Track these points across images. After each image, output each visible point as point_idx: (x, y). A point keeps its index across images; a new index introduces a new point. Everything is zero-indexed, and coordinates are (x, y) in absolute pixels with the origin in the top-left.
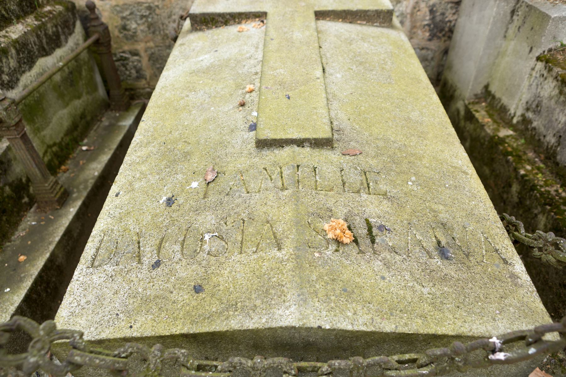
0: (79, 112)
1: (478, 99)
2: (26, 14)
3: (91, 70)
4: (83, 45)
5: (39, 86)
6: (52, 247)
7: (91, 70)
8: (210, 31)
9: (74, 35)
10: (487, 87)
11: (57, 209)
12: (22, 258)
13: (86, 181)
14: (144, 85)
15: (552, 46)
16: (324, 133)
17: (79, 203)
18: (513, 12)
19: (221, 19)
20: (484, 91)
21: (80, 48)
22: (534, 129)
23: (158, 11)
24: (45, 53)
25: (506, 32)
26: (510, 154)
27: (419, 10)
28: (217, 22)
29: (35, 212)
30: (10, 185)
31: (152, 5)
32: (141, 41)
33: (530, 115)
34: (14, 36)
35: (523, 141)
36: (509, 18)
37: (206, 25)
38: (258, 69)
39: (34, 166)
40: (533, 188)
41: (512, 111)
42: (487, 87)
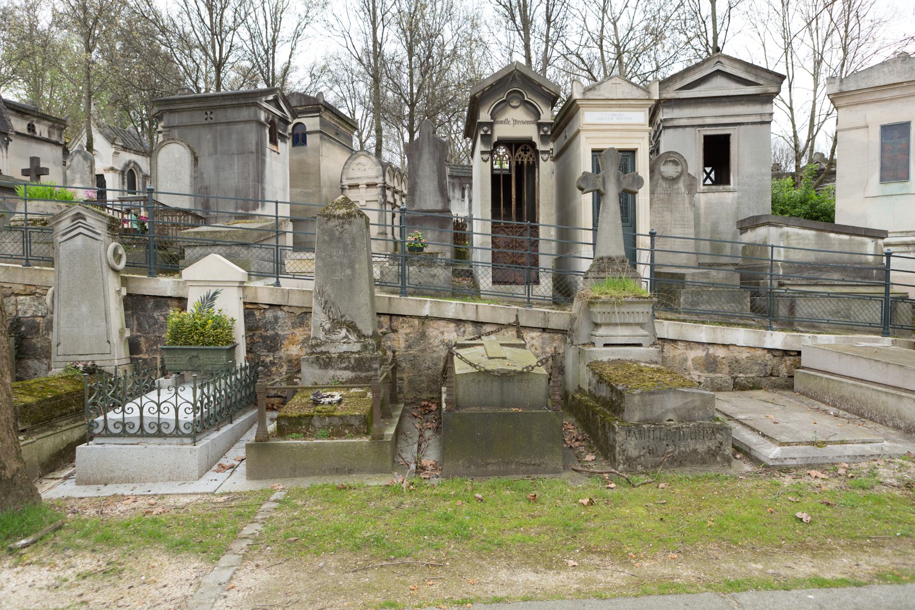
1: (577, 392)
42: (579, 386)
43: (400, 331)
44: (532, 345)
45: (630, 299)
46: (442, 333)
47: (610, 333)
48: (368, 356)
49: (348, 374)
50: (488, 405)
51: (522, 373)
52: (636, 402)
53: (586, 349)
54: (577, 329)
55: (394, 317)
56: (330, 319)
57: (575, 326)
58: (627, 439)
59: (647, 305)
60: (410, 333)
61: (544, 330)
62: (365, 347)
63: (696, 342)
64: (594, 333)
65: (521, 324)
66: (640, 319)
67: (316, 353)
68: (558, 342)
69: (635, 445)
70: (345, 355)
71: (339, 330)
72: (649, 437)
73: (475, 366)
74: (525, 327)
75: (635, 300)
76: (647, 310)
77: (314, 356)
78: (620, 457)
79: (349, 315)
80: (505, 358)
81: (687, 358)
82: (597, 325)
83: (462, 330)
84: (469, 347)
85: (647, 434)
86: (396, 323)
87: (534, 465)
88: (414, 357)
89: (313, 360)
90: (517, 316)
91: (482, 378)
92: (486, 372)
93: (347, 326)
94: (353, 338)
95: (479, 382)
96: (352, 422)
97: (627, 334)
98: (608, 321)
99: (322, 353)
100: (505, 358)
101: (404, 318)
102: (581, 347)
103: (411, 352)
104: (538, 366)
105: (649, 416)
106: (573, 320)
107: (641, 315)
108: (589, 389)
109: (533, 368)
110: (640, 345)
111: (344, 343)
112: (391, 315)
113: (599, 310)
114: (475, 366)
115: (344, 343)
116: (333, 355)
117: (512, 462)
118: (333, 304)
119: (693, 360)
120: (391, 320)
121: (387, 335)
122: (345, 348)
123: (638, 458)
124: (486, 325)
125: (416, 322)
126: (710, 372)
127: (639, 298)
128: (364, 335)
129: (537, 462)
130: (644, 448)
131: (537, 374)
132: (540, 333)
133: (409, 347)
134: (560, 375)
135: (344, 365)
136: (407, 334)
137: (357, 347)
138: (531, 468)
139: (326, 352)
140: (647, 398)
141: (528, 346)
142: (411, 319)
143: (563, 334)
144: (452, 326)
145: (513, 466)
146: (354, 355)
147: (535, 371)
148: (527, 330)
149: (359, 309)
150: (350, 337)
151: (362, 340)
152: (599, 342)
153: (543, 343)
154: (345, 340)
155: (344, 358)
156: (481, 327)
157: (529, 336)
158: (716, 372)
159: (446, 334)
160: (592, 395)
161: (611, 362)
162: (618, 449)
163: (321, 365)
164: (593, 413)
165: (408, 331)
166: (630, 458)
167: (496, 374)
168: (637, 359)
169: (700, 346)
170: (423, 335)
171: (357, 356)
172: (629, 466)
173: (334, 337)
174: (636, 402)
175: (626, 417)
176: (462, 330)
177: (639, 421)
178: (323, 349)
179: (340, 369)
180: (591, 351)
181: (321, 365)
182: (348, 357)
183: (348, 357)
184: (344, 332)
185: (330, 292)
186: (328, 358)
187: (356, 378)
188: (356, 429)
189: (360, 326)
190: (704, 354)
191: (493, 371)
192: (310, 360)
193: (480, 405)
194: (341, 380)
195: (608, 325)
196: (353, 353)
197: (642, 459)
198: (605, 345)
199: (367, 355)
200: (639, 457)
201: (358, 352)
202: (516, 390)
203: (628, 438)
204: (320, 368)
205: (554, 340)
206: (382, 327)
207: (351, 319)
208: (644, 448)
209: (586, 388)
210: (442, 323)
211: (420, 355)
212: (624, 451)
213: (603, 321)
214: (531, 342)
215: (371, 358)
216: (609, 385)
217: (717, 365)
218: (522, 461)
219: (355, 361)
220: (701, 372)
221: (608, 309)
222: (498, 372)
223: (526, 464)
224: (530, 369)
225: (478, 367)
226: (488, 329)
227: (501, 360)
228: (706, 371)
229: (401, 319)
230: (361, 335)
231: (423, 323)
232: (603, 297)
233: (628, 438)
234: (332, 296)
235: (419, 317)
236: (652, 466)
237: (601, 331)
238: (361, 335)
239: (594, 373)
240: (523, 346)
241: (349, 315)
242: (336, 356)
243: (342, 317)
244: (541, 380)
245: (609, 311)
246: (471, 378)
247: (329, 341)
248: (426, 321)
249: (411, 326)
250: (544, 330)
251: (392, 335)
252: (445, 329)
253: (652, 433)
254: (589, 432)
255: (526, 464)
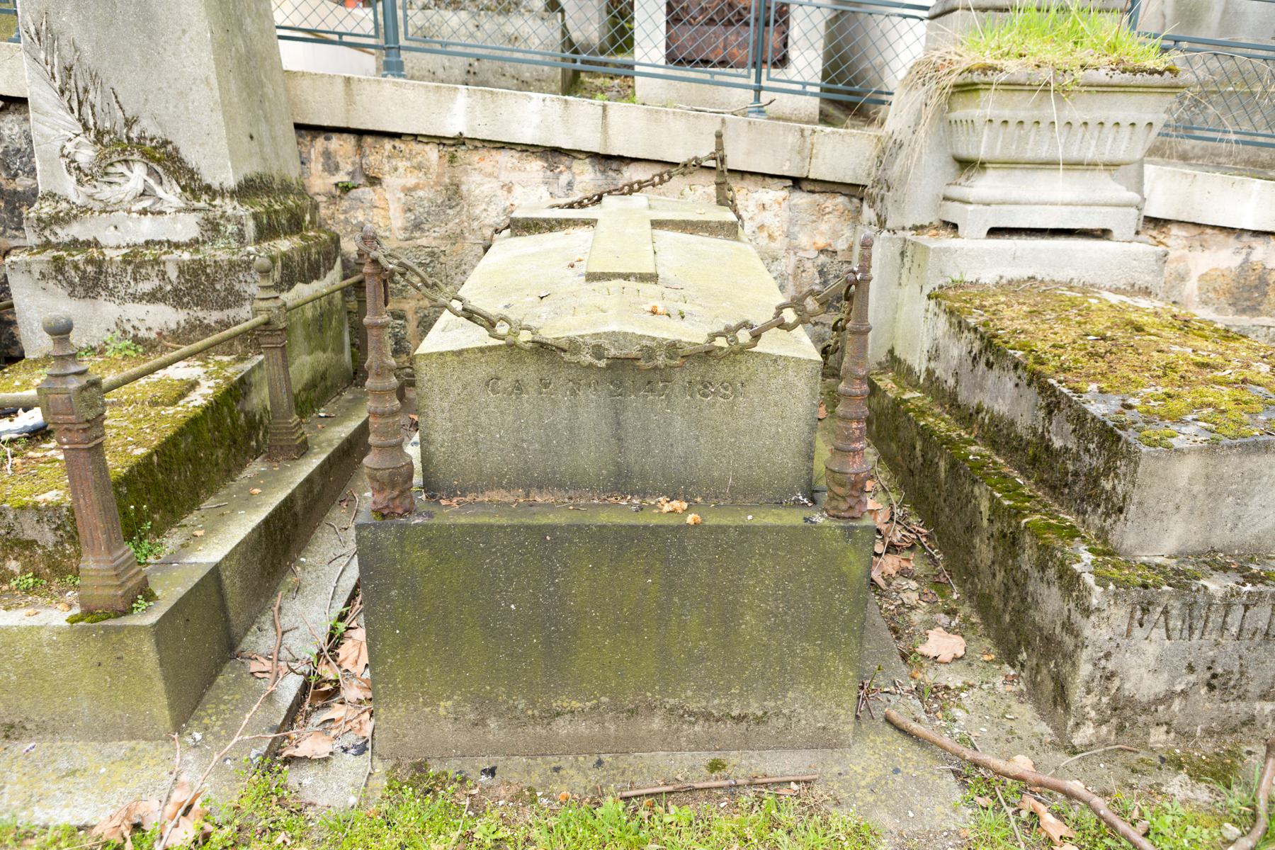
0: (321, 369)
1: (883, 368)
2: (292, 233)
3: (341, 323)
4: (340, 284)
5: (304, 304)
6: (294, 486)
7: (341, 323)
8: (532, 237)
9: (332, 272)
10: (891, 352)
11: (294, 459)
12: (257, 491)
13: (330, 442)
14: (403, 363)
15: (942, 282)
16: (648, 269)
17: (323, 457)
18: (902, 254)
19: (545, 225)
20: (889, 358)
21: (335, 287)
22: (938, 378)
23: (443, 259)
24: (306, 281)
25: (900, 278)
26: (913, 410)
27: (804, 271)
28: (541, 228)
29: (263, 461)
30: (246, 415)
31: (436, 249)
32: (412, 298)
33: (932, 365)
34: (284, 249)
35: (929, 399)
36: (899, 261)
37: (528, 232)
38: (588, 251)
39: (284, 390)
40: (932, 433)
41: (917, 369)
42: (891, 352)
43: (388, 180)
44: (761, 227)
45: (1101, 76)
46: (508, 188)
47: (1015, 194)
48: (223, 256)
49: (163, 317)
50: (561, 486)
51: (706, 355)
52: (1182, 483)
53: (925, 239)
54: (903, 179)
55: (369, 140)
56: (86, 128)
57: (895, 172)
58: (1129, 634)
59: (1152, 99)
60: (416, 187)
61: (797, 183)
62: (213, 227)
63: (1222, 229)
64: (954, 191)
65: (731, 164)
66: (1123, 147)
67: (57, 247)
68: (833, 218)
69: (1159, 659)
70: (149, 254)
71: (121, 168)
72: (1224, 627)
73: (490, 324)
74: (743, 173)
75: (1118, 78)
76: (1149, 118)
77: (50, 254)
78: (1091, 699)
79: (154, 117)
80: (652, 278)
81: (1187, 272)
82: (966, 165)
83: (564, 178)
84: (551, 229)
85: (1216, 618)
86: (379, 156)
87: (740, 719)
88: (432, 254)
89: (44, 268)
90: (719, 136)
91: (530, 372)
92: (542, 348)
93: (144, 154)
94: (170, 194)
95: (519, 387)
96: (30, 534)
97: (1069, 196)
98: (1013, 153)
99: (75, 244)
100: (652, 278)
101: (397, 143)
102: (909, 235)
103: (423, 241)
104: (782, 325)
105: (1220, 538)
106: (887, 153)
107: (1125, 131)
108: (930, 373)
109: (756, 337)
110: (1104, 234)
111: (144, 212)
112: (360, 133)
113: (989, 112)
114: (490, 324)
115: (144, 212)
116: (109, 253)
117: (651, 709)
118: (94, 77)
119: (1202, 278)
120: (359, 146)
121: (353, 193)
122: (147, 229)
123: (1159, 701)
124: (633, 166)
125: (432, 153)
126: (1243, 311)
127: (1134, 72)
128: (208, 189)
129: (755, 708)
130: (1191, 669)
131: (775, 359)
132: (785, 193)
133: (417, 226)
134: (1184, 798)
135: (146, 287)
136: (408, 191)
137: (186, 227)
138: (726, 728)
139: (88, 244)
140: (1231, 465)
141: (749, 227)
142: (416, 147)
143: (851, 196)
144: (536, 166)
145: (657, 723)
146: (177, 253)
147: (771, 344)
148: (749, 183)
149: (182, 95)
150: (159, 191)
151: (202, 204)
152: (975, 221)
153: (792, 222)
154: (146, 203)
155: (142, 264)
156: (618, 171)
157: (750, 197)
158: (1260, 313)
159: (517, 190)
160: (932, 384)
161: (1011, 287)
162: (1085, 669)
163: (71, 284)
164: (953, 466)
165: (411, 181)
166: (1130, 701)
167: (587, 358)
168: (1088, 278)
169: (1232, 240)
170: (454, 193)
171: (186, 256)
172: (1121, 729)
173: (106, 192)
174: (1182, 483)
175: (1127, 534)
176: (564, 178)
177: (1180, 555)
178: (77, 231)
179: (136, 298)
180: (946, 250)
181: (71, 284)
182: (156, 262)
183: (156, 262)
184: (137, 175)
185: (75, 32)
186: (90, 261)
187: (197, 328)
188: (50, 556)
189: (191, 156)
190: (1239, 260)
191: (574, 346)
192: (36, 269)
193: (529, 481)
194: (143, 333)
195: (1011, 164)
196: (177, 246)
197: (1177, 705)
198: (994, 232)
199: (219, 253)
200: (1168, 697)
201: (193, 244)
202: (679, 424)
203: (1138, 632)
204: (71, 295)
205: (822, 212)
206: (337, 168)
207: (159, 133)
208: (1191, 669)
209: (919, 363)
210: (505, 157)
211: (448, 249)
212: (1109, 677)
213: (998, 153)
214: (759, 220)
215: (232, 265)
216: (1036, 379)
217: (1265, 294)
218: (693, 706)
219: (181, 272)
220: (1217, 310)
221: (1020, 107)
222: (598, 352)
223: (708, 716)
224: (744, 336)
225: (502, 329)
226: (633, 174)
227: (632, 284)
228: (1231, 310)
229: (388, 144)
230: (194, 187)
231: (453, 159)
232: (1013, 67)
233: (1138, 632)
234: (86, 47)
235: (440, 140)
236: (1209, 732)
237: (983, 186)
238: (194, 187)
239: (961, 326)
240: (730, 230)
241: (154, 117)
242: (116, 255)
243: (129, 123)
244: (789, 386)
245: (1021, 115)
246: (483, 372)
247: (97, 206)
248: (461, 153)
249: (419, 167)
250: (797, 183)
251: (366, 193)
252: (514, 177)
253: (1238, 612)
254: (931, 519)
255: (708, 716)
